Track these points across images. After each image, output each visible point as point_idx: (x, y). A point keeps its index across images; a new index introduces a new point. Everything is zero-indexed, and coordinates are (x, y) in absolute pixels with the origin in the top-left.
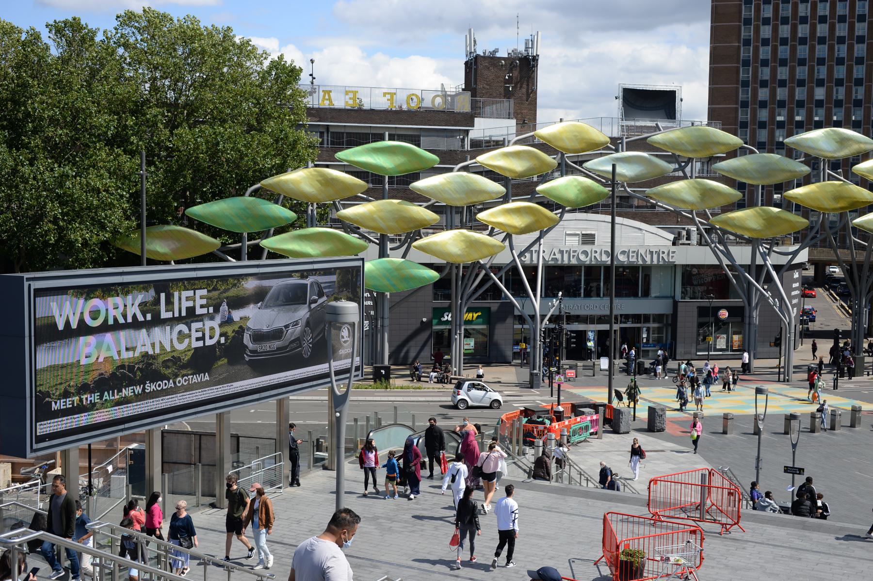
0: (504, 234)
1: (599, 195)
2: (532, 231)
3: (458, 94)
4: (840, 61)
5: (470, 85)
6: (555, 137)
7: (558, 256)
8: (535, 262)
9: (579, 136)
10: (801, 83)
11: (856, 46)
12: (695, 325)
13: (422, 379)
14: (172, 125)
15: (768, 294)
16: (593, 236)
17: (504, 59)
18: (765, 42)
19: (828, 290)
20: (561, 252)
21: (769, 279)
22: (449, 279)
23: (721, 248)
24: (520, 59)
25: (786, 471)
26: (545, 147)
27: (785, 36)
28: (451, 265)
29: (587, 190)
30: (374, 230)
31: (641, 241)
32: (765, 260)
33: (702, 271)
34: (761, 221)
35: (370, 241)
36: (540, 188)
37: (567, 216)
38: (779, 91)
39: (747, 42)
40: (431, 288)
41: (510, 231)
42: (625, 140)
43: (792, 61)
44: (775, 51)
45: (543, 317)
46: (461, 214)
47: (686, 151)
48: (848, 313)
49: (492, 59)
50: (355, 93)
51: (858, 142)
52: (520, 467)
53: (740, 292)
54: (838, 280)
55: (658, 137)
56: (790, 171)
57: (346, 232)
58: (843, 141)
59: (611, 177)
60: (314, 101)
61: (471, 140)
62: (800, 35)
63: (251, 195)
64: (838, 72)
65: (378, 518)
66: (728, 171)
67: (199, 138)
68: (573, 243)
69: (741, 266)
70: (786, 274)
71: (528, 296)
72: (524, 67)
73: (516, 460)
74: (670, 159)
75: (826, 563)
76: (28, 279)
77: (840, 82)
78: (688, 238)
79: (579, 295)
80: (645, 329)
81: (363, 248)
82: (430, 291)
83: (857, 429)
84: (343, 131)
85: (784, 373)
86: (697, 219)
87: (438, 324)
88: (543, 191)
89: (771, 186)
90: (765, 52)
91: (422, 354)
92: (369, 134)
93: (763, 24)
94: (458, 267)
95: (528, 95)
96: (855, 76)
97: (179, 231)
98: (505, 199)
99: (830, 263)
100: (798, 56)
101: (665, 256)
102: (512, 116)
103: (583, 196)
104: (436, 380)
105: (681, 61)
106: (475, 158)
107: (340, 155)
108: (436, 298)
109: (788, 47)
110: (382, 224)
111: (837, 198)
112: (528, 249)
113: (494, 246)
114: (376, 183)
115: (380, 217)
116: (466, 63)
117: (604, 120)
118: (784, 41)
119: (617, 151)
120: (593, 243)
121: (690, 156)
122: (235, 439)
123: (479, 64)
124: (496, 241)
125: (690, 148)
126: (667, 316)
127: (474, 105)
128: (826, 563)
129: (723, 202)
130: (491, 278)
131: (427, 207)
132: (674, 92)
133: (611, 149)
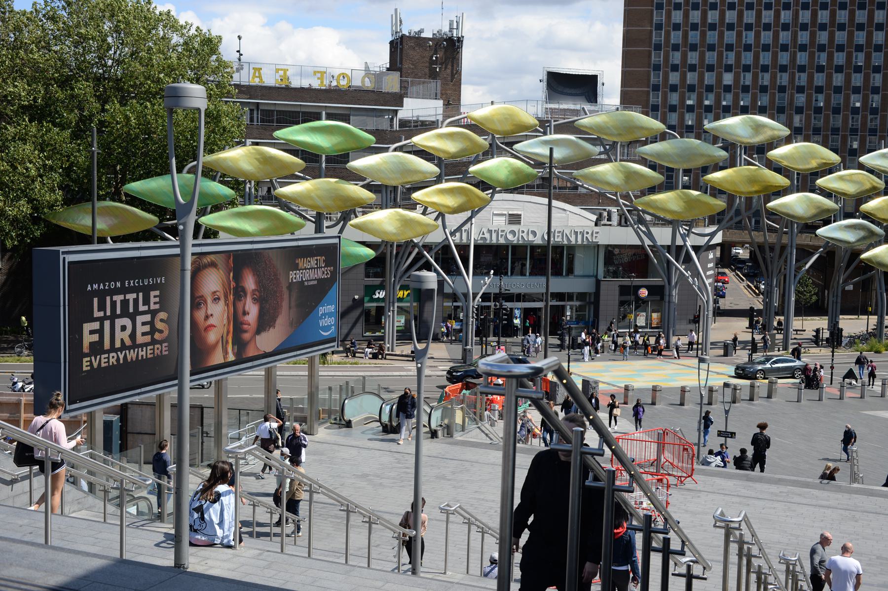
0: (435, 214)
1: (529, 176)
2: (464, 211)
3: (382, 73)
4: (748, 48)
5: (395, 65)
6: (487, 119)
7: (487, 236)
8: (465, 240)
9: (509, 117)
10: (710, 68)
11: (763, 33)
12: (617, 303)
13: (357, 355)
14: (103, 100)
15: (687, 274)
16: (519, 216)
17: (429, 39)
18: (677, 27)
19: (733, 271)
20: (490, 232)
21: (688, 260)
22: (386, 259)
23: (644, 229)
24: (445, 40)
25: (719, 435)
26: (476, 127)
27: (696, 21)
28: (385, 243)
29: (517, 172)
30: (313, 207)
31: (573, 222)
32: (685, 241)
33: (623, 251)
34: (682, 204)
35: (305, 218)
36: (472, 169)
37: (497, 196)
38: (689, 75)
39: (659, 27)
40: (363, 267)
41: (443, 210)
42: (553, 123)
43: (702, 46)
44: (685, 36)
45: (475, 295)
46: (394, 194)
47: (612, 135)
48: (755, 292)
49: (417, 40)
50: (285, 71)
51: (773, 129)
52: (483, 431)
53: (661, 271)
54: (743, 262)
55: (585, 121)
56: (709, 156)
57: (281, 209)
58: (758, 127)
59: (547, 161)
60: (243, 78)
61: (400, 120)
62: (710, 21)
63: (188, 172)
64: (746, 58)
65: (367, 475)
66: (651, 155)
67: (130, 113)
68: (500, 223)
69: (662, 246)
70: (704, 254)
71: (460, 274)
72: (449, 48)
73: (480, 425)
74: (594, 142)
75: (771, 508)
76: (64, 253)
77: (747, 68)
78: (609, 219)
79: (525, 275)
80: (568, 307)
81: (301, 226)
82: (362, 269)
83: (773, 400)
84: (272, 108)
85: (702, 349)
86: (621, 201)
87: (369, 301)
88: (473, 172)
89: (698, 169)
90: (676, 37)
91: (354, 331)
92: (299, 112)
93: (675, 9)
94: (392, 246)
95: (453, 76)
96: (761, 63)
97: (116, 207)
98: (439, 180)
99: (734, 244)
100: (708, 42)
101: (589, 236)
102: (439, 96)
103: (513, 177)
104: (371, 356)
105: (597, 45)
106: (410, 138)
107: (278, 133)
108: (367, 275)
109: (698, 33)
110: (319, 203)
111: (752, 180)
112: (459, 229)
113: (428, 225)
114: (312, 162)
115: (319, 197)
116: (391, 43)
117: (529, 103)
118: (694, 27)
119: (545, 133)
120: (519, 223)
121: (615, 140)
122: (198, 412)
123: (404, 44)
124: (429, 220)
125: (616, 132)
126: (590, 294)
127: (404, 86)
128: (771, 508)
129: (647, 185)
130: (424, 256)
131: (363, 186)
132: (595, 77)
133: (540, 132)
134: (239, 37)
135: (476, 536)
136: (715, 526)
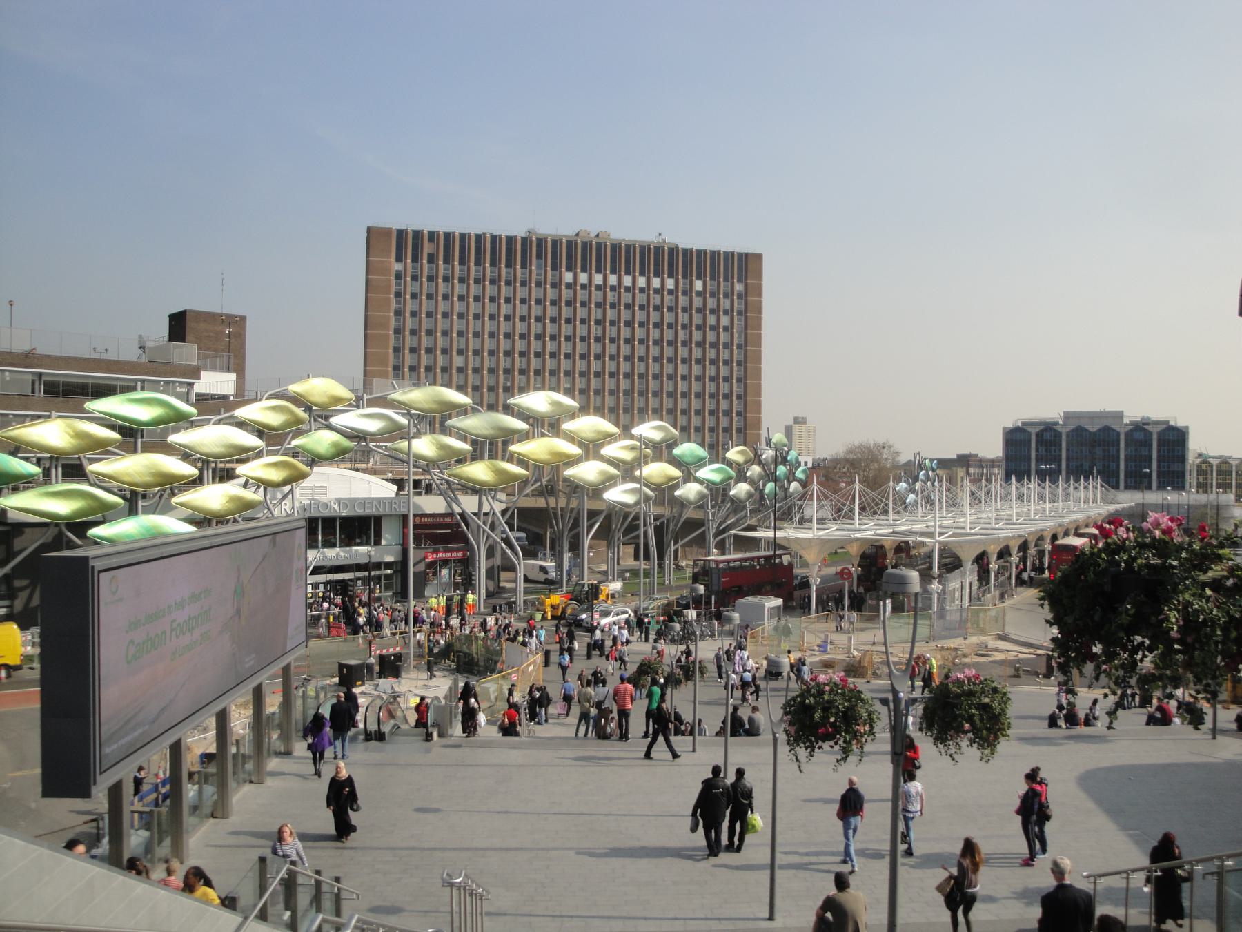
114: (131, 436)
134: (11, 303)
135: (455, 891)
136: (739, 849)
